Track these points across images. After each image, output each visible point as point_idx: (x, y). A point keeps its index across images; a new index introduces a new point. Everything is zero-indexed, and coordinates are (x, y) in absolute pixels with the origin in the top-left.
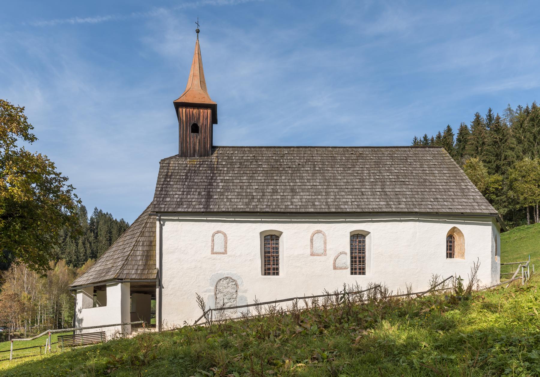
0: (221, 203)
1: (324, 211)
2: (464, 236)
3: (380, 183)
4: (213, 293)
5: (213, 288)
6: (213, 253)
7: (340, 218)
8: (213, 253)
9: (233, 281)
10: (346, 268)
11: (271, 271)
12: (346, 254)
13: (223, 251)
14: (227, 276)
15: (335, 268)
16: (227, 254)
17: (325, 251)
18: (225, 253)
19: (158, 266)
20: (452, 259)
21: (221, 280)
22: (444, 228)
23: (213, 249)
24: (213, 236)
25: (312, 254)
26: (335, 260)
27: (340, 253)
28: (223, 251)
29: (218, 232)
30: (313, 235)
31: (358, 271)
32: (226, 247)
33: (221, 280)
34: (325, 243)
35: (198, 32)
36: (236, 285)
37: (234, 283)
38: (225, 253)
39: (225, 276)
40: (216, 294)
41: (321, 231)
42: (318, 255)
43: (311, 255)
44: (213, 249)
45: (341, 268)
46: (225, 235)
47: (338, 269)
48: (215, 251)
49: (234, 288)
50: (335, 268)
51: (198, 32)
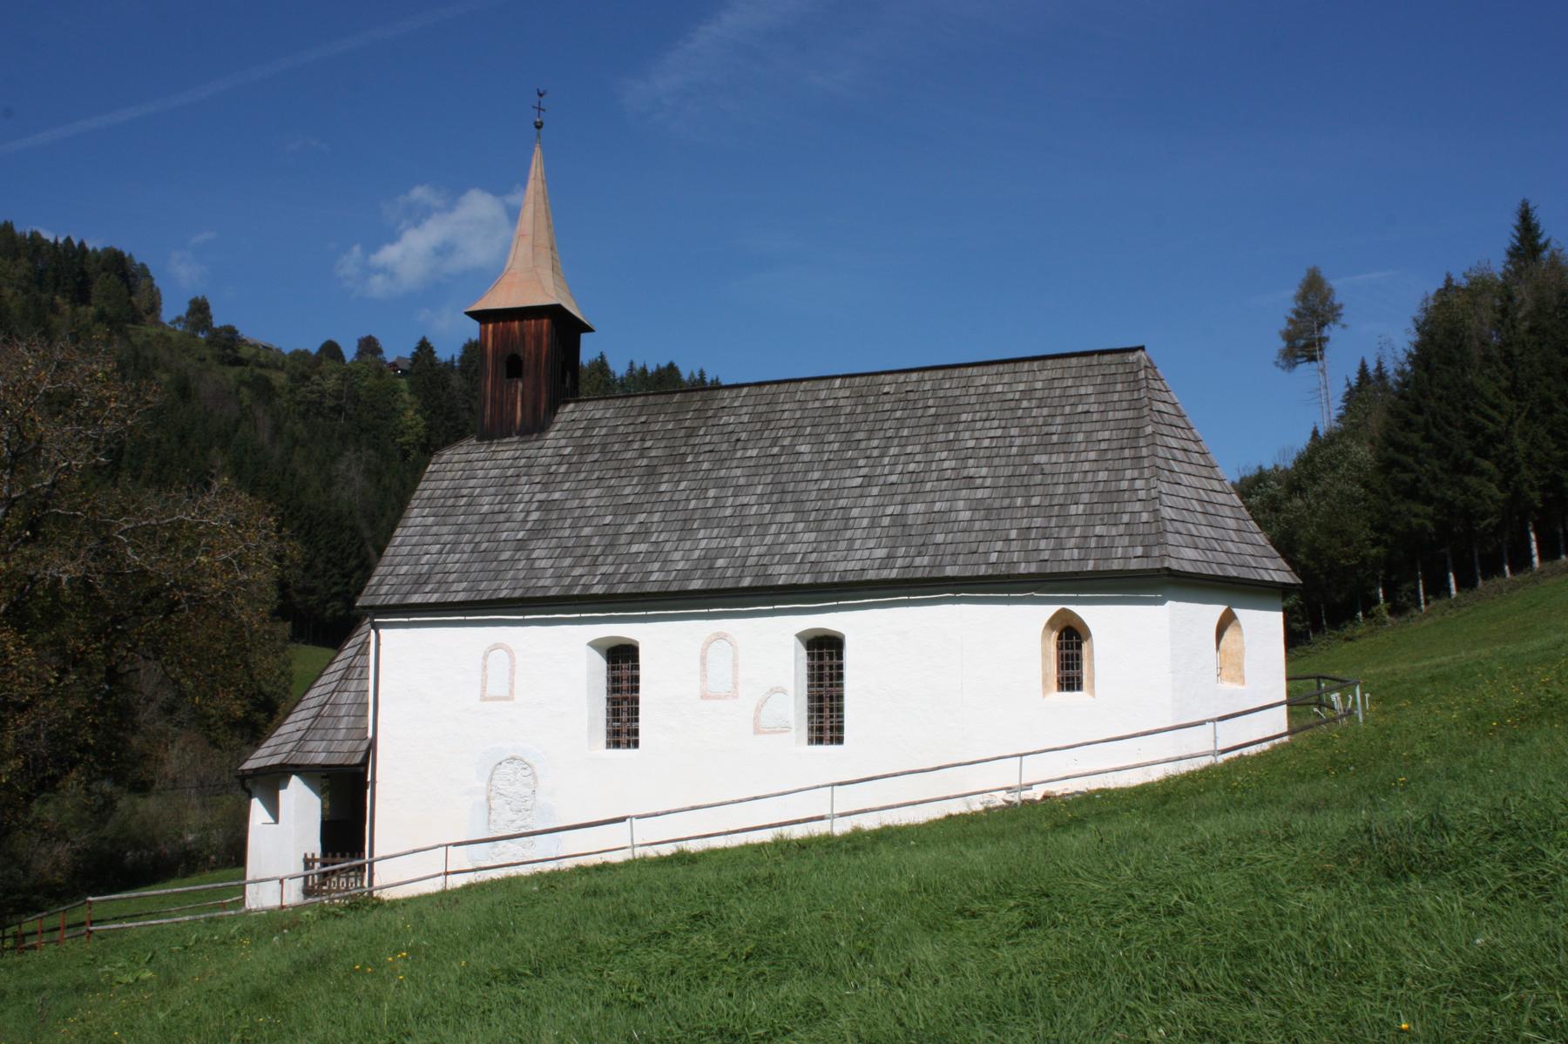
0: (1019, 557)
1: (1048, 571)
2: (1243, 627)
3: (790, 507)
4: (484, 798)
5: (484, 785)
6: (484, 699)
7: (897, 591)
8: (484, 699)
9: (526, 766)
10: (785, 729)
11: (624, 738)
12: (784, 692)
13: (506, 693)
14: (513, 754)
15: (757, 731)
16: (513, 699)
17: (735, 685)
18: (509, 697)
19: (370, 734)
20: (1076, 693)
21: (500, 764)
22: (1216, 611)
23: (484, 688)
24: (485, 657)
25: (704, 697)
26: (758, 710)
27: (771, 690)
28: (506, 693)
29: (496, 647)
30: (708, 644)
31: (828, 734)
32: (512, 684)
33: (500, 764)
34: (735, 666)
35: (539, 126)
36: (533, 774)
37: (527, 772)
38: (509, 697)
39: (508, 756)
40: (488, 799)
41: (726, 635)
42: (718, 698)
43: (702, 697)
44: (484, 688)
45: (773, 731)
46: (510, 652)
47: (764, 733)
48: (489, 692)
49: (526, 785)
50: (757, 731)
51: (539, 126)
